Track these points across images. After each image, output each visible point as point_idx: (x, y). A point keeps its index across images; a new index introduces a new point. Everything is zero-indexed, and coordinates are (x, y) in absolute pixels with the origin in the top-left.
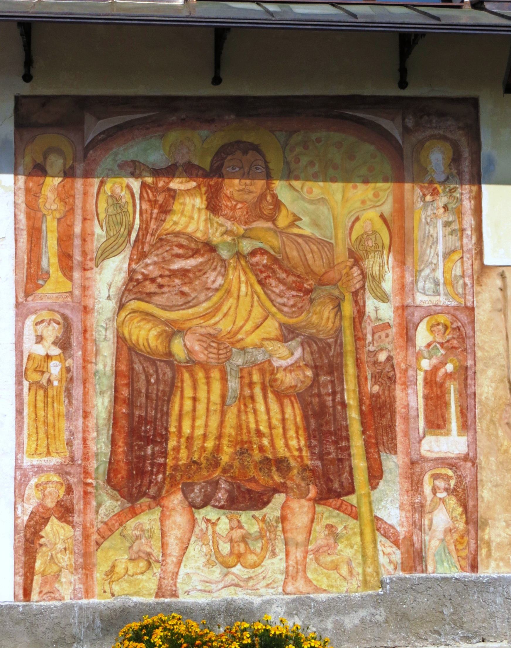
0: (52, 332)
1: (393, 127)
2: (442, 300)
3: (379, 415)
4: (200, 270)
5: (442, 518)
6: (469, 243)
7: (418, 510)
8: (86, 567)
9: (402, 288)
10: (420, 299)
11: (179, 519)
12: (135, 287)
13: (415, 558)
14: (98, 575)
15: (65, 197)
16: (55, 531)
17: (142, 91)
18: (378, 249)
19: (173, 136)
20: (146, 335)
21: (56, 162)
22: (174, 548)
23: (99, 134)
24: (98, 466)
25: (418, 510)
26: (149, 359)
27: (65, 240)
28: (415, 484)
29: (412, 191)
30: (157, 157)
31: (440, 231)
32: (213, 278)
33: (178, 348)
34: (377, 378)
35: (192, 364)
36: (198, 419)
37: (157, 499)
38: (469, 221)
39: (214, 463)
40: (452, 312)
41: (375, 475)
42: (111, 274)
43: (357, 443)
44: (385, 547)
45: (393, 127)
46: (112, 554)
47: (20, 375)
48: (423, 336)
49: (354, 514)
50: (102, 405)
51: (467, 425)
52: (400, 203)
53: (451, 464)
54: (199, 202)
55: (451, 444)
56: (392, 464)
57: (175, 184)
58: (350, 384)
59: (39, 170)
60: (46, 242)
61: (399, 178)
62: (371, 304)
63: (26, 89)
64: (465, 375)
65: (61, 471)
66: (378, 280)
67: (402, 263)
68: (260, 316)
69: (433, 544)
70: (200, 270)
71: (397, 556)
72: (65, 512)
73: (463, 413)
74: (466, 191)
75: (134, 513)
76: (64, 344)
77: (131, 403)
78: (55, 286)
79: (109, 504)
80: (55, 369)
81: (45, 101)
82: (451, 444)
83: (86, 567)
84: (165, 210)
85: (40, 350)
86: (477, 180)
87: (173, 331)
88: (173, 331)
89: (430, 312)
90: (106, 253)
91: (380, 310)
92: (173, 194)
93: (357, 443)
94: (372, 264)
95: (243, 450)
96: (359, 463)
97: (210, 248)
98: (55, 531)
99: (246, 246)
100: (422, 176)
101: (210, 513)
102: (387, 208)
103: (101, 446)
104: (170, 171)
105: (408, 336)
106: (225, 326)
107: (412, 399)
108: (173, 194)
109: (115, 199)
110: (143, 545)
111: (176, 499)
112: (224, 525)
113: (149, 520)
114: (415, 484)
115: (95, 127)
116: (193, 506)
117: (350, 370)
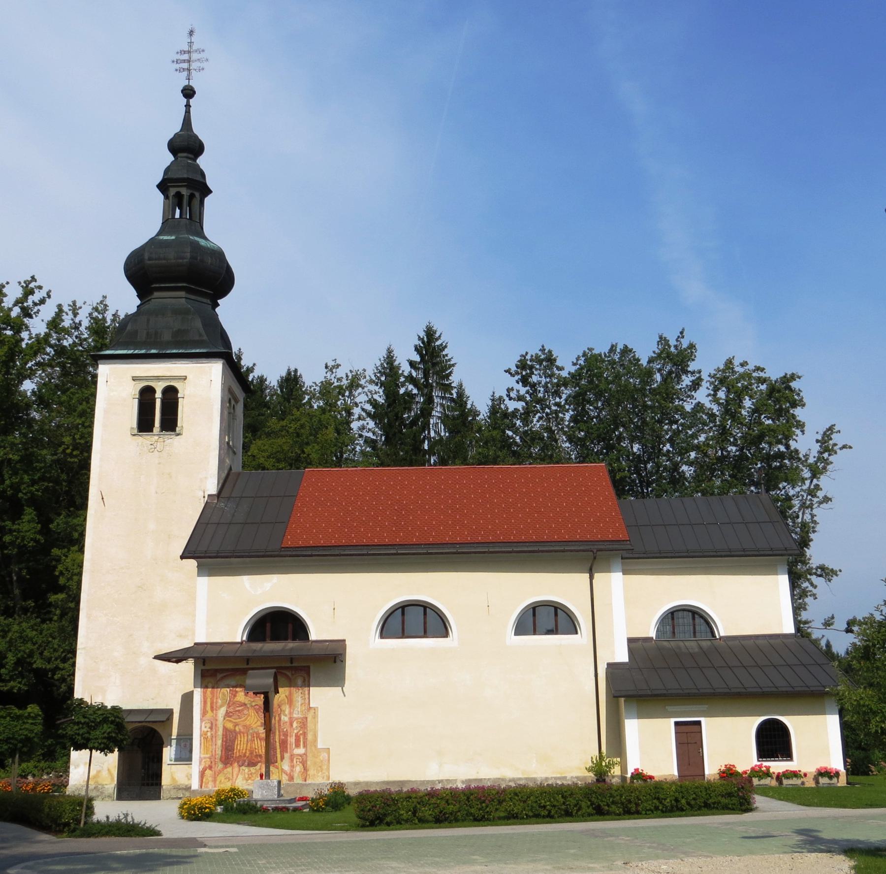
0: (209, 725)
1: (289, 674)
2: (300, 716)
3: (284, 744)
4: (242, 710)
5: (298, 768)
6: (307, 701)
7: (292, 766)
8: (215, 781)
9: (290, 713)
10: (295, 716)
11: (236, 769)
12: (228, 714)
13: (291, 778)
14: (217, 783)
15: (212, 693)
16: (208, 772)
17: (230, 667)
18: (285, 703)
19: (238, 678)
20: (230, 726)
21: (210, 685)
22: (235, 776)
23: (115, 870)
24: (218, 757)
25: (292, 766)
26: (230, 731)
27: (212, 703)
28: (292, 761)
29: (293, 690)
30: (233, 683)
31: (300, 699)
32: (246, 712)
33: (237, 729)
34: (284, 735)
35: (240, 732)
36: (241, 746)
37: (231, 764)
38: (307, 696)
39: (245, 756)
40: (302, 719)
41: (282, 758)
42: (222, 711)
43: (278, 751)
44: (284, 775)
45: (289, 674)
46: (221, 778)
47: (201, 736)
48: (295, 725)
49: (277, 768)
50: (219, 742)
51: (305, 746)
52: (290, 692)
53: (300, 756)
54: (243, 694)
55: (301, 751)
56: (287, 756)
57: (238, 689)
58: (277, 737)
59: (206, 687)
60: (290, 556)
61: (290, 686)
62: (282, 717)
63: (203, 668)
64: (305, 734)
65: (210, 758)
66: (284, 711)
67: (290, 707)
68: (136, 821)
69: (296, 775)
70: (242, 710)
71: (287, 778)
72: (210, 768)
73: (304, 743)
74: (306, 689)
75: (226, 768)
76: (211, 728)
77: (226, 742)
78: (210, 714)
79: (221, 766)
80: (209, 734)
81: (208, 670)
82: (301, 751)
83: (215, 781)
84: (235, 696)
85: (206, 730)
86: (309, 686)
87: (236, 725)
88: (236, 725)
89: (297, 719)
90: (222, 706)
91: (285, 718)
92: (237, 692)
93: (278, 751)
94: (283, 708)
95: (251, 753)
96: (279, 756)
97: (245, 705)
98: (208, 772)
99: (254, 704)
100: (295, 685)
101: (243, 767)
102: (287, 694)
103: (219, 752)
104: (236, 687)
105: (291, 725)
106: (248, 723)
107: (292, 740)
108: (237, 692)
109: (223, 694)
110: (228, 775)
111: (236, 764)
112: (247, 770)
113: (229, 769)
114: (292, 761)
115: (219, 676)
116: (240, 766)
117: (277, 733)
